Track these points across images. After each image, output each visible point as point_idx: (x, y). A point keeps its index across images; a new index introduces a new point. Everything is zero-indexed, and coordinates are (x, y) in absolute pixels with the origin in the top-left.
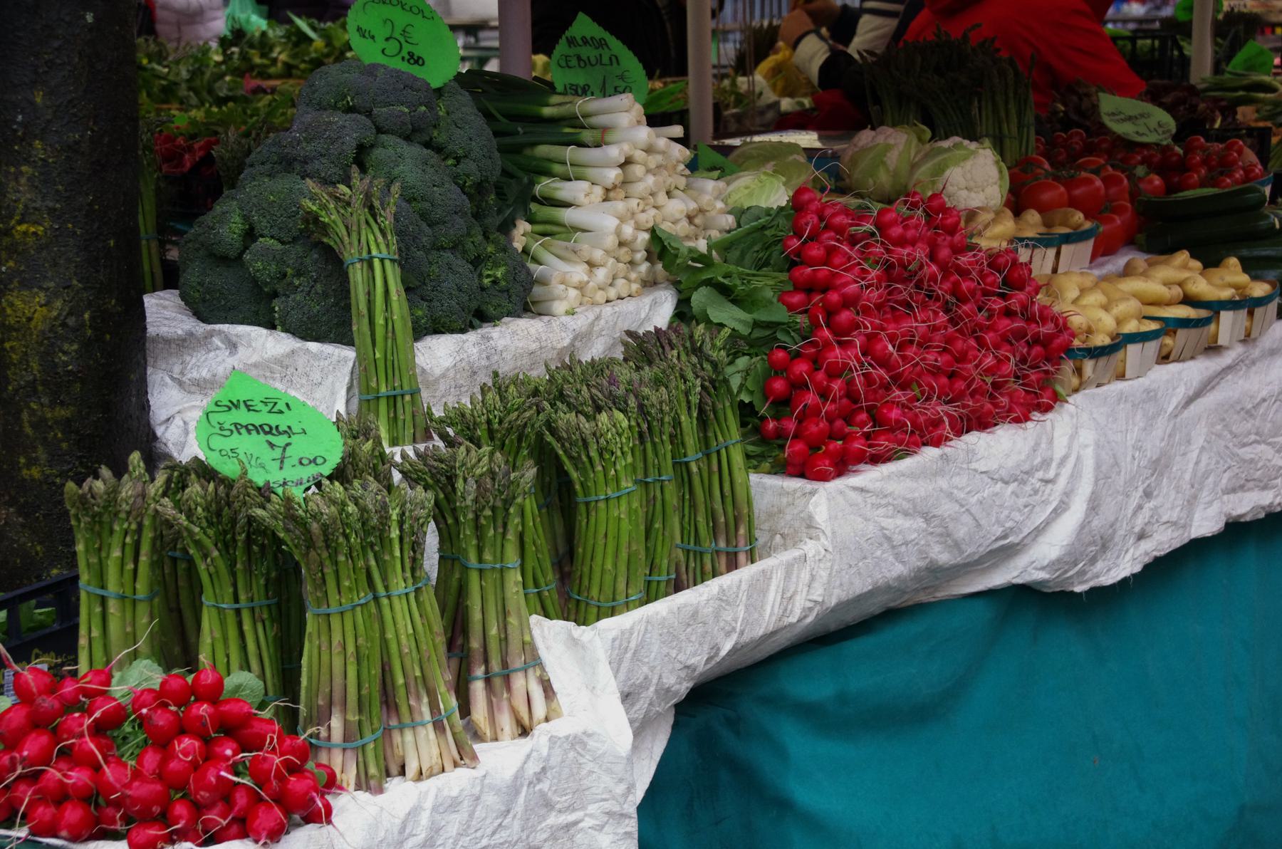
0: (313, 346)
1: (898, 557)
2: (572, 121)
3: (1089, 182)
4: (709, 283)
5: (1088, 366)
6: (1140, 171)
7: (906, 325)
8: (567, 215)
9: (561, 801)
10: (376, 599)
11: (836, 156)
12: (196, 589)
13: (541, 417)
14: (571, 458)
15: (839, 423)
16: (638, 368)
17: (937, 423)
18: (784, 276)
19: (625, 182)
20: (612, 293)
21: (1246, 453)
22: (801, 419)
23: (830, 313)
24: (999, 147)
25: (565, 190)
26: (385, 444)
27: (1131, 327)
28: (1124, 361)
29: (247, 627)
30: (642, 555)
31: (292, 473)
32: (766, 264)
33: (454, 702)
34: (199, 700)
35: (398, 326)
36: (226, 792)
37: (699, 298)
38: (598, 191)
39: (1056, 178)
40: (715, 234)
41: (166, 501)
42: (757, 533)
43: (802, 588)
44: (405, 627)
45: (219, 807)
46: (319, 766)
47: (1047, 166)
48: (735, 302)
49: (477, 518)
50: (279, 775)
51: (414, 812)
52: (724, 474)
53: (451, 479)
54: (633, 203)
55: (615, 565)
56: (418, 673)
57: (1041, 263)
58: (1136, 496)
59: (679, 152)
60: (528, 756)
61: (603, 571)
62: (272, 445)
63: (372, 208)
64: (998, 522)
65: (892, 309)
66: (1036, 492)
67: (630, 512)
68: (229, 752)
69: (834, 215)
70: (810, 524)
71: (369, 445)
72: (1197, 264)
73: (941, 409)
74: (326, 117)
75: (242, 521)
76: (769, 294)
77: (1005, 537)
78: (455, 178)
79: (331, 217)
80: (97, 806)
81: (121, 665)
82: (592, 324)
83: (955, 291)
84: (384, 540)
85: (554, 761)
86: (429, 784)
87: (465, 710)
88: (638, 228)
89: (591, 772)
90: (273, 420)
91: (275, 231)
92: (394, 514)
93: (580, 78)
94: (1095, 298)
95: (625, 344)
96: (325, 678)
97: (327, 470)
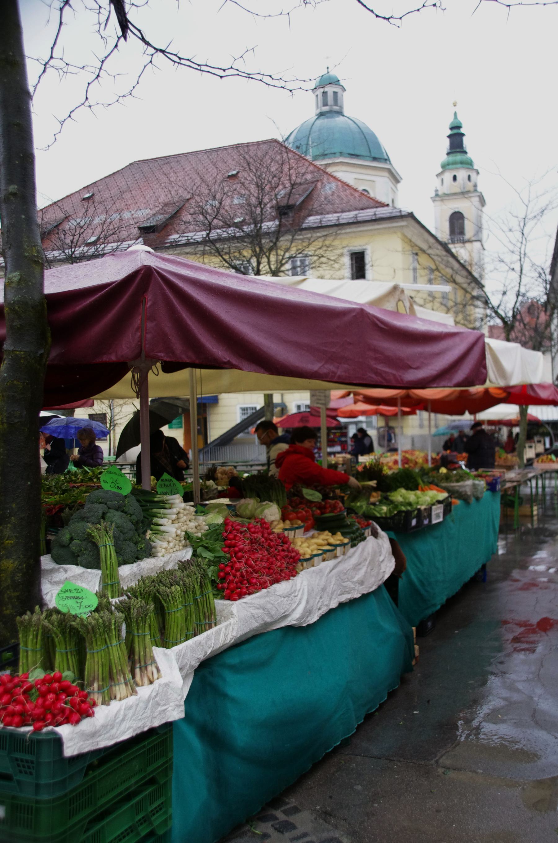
0: (89, 570)
1: (256, 621)
2: (163, 502)
3: (301, 512)
4: (202, 546)
5: (305, 564)
6: (314, 509)
7: (256, 555)
8: (162, 528)
9: (162, 703)
10: (108, 647)
11: (235, 506)
12: (54, 646)
13: (156, 588)
14: (164, 600)
15: (239, 584)
16: (183, 572)
17: (265, 583)
18: (223, 543)
19: (178, 518)
20: (175, 550)
21: (345, 584)
22: (228, 584)
23: (236, 553)
24: (278, 504)
25: (161, 521)
26: (110, 598)
27: (315, 552)
28: (314, 562)
29: (69, 657)
30: (185, 627)
31: (82, 610)
32: (218, 540)
33: (130, 676)
34: (56, 682)
35: (114, 564)
36: (63, 710)
37: (199, 550)
38: (170, 521)
39: (293, 512)
40: (203, 531)
41: (46, 621)
42: (217, 617)
43: (230, 633)
44: (116, 655)
45: (61, 715)
46: (91, 699)
47: (290, 508)
48: (210, 551)
49: (137, 620)
50: (79, 704)
51: (119, 711)
52: (208, 602)
53: (129, 609)
54: (180, 524)
55: (177, 630)
56: (120, 668)
57: (290, 535)
58: (318, 598)
59: (193, 509)
60: (152, 691)
61: (173, 632)
62: (77, 602)
63: (106, 531)
64: (283, 609)
65: (252, 551)
66: (292, 599)
67: (181, 615)
68: (64, 697)
69: (236, 526)
70: (232, 614)
71: (106, 600)
72: (330, 534)
73: (267, 578)
74: (94, 505)
75: (68, 626)
76: (219, 548)
77: (284, 613)
78: (130, 521)
79: (95, 534)
80: (24, 716)
81: (32, 671)
82: (169, 559)
83: (269, 545)
84: (110, 629)
85: (160, 691)
86: (124, 702)
87: (134, 677)
88: (182, 531)
89: (171, 693)
90: (78, 595)
91: (79, 538)
92: (113, 621)
93: (164, 490)
94: (305, 545)
95: (178, 564)
96: (92, 672)
97: (93, 609)
